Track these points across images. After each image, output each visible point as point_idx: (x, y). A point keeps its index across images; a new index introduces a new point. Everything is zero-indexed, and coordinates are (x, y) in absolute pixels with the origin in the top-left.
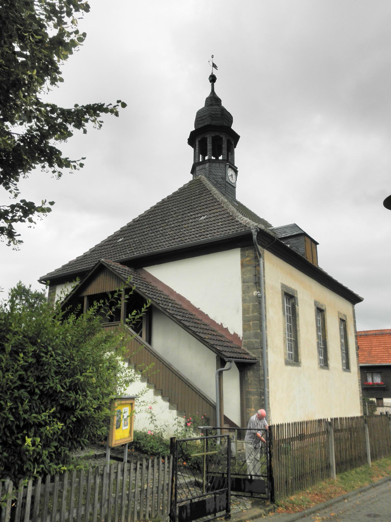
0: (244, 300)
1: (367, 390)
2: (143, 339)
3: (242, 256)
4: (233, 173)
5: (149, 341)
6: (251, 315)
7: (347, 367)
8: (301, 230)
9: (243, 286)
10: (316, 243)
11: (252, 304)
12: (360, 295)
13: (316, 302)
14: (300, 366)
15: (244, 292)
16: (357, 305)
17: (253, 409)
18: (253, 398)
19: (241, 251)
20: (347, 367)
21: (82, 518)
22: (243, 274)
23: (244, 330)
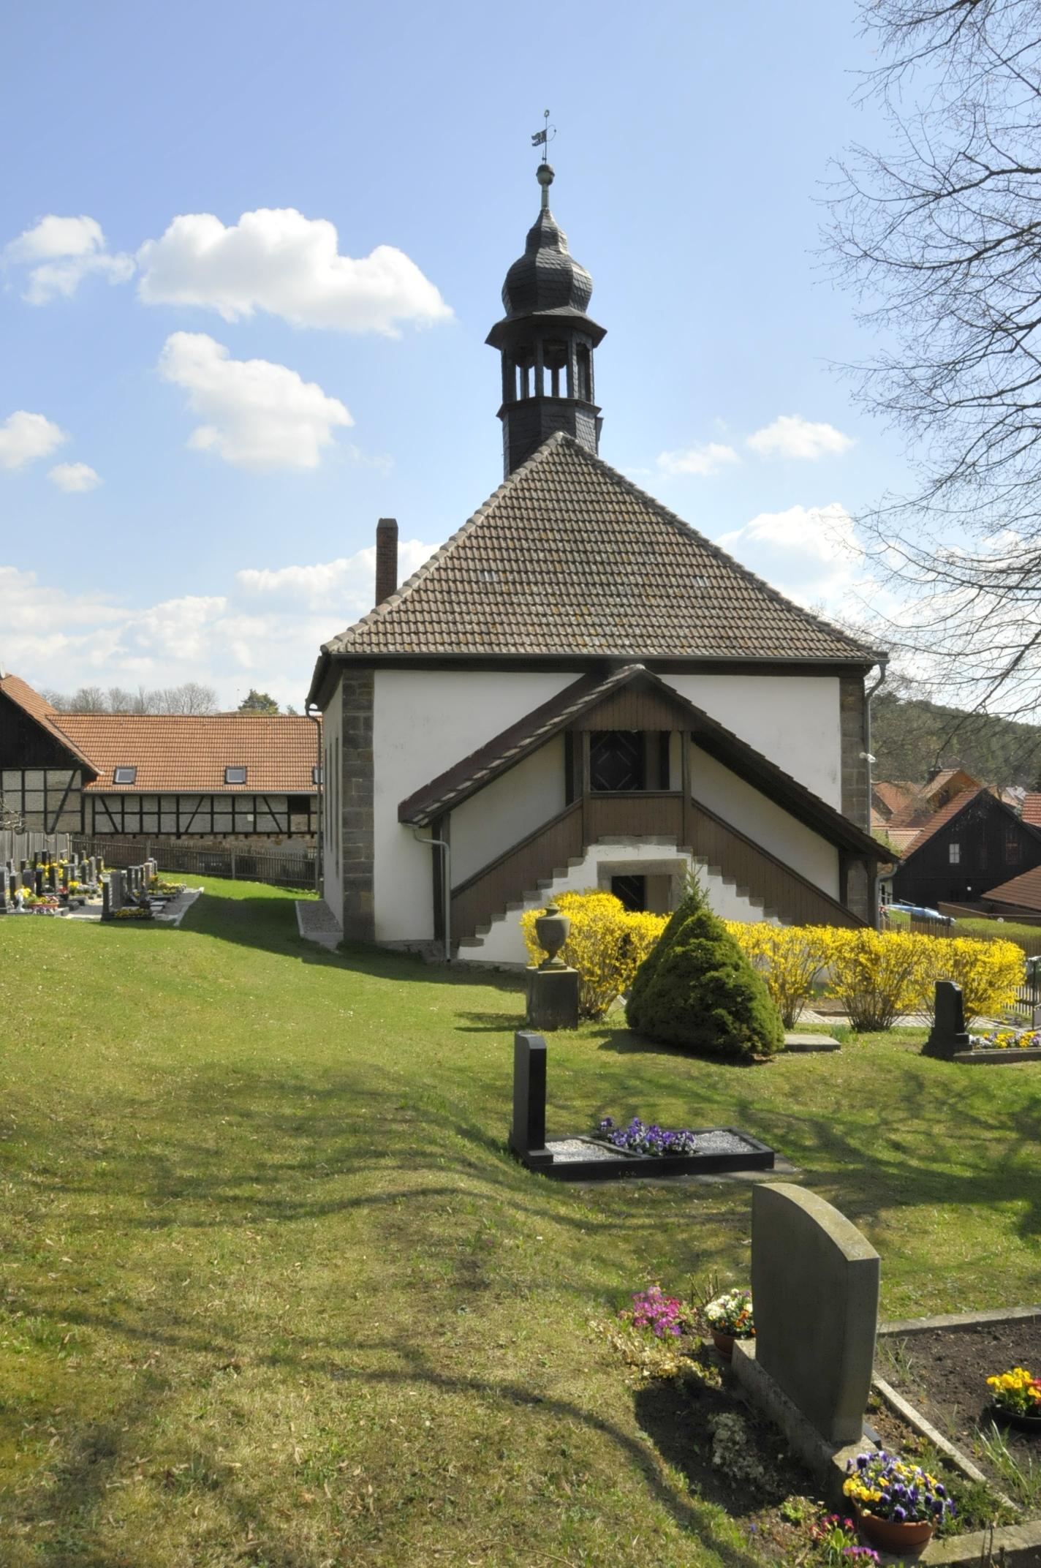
6: (854, 787)
9: (843, 741)
14: (381, 521)
15: (844, 751)
19: (841, 683)
22: (843, 721)
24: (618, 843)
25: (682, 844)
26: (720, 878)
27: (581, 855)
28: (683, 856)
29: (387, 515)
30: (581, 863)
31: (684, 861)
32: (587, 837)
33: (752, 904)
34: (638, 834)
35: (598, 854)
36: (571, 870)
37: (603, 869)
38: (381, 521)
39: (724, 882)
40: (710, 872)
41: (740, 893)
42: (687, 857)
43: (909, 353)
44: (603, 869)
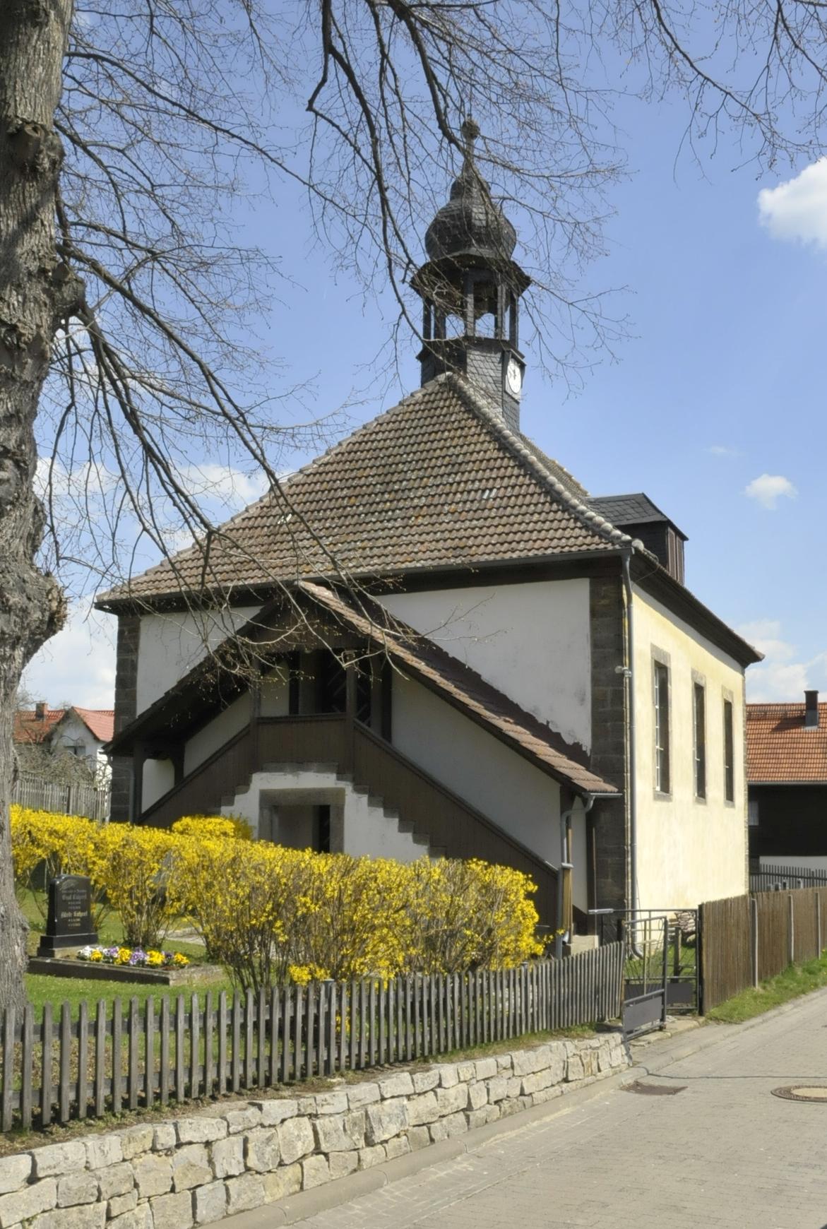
0: (595, 681)
1: (763, 841)
2: (374, 731)
3: (594, 595)
4: (518, 370)
5: (387, 732)
6: (609, 708)
7: (730, 795)
8: (659, 512)
9: (593, 653)
10: (684, 538)
11: (611, 688)
12: (758, 646)
13: (693, 672)
14: (670, 800)
15: (595, 665)
16: (752, 669)
17: (610, 880)
18: (610, 861)
19: (592, 584)
20: (730, 795)
21: (811, 973)
22: (594, 629)
23: (595, 736)
24: (280, 770)
25: (341, 775)
26: (381, 811)
27: (244, 783)
28: (341, 784)
29: (701, 807)
30: (246, 791)
31: (340, 793)
32: (258, 766)
33: (416, 841)
34: (299, 762)
35: (262, 782)
36: (237, 798)
37: (270, 802)
38: (670, 800)
39: (386, 815)
40: (370, 804)
41: (403, 828)
42: (348, 787)
43: (367, 67)
44: (270, 802)
